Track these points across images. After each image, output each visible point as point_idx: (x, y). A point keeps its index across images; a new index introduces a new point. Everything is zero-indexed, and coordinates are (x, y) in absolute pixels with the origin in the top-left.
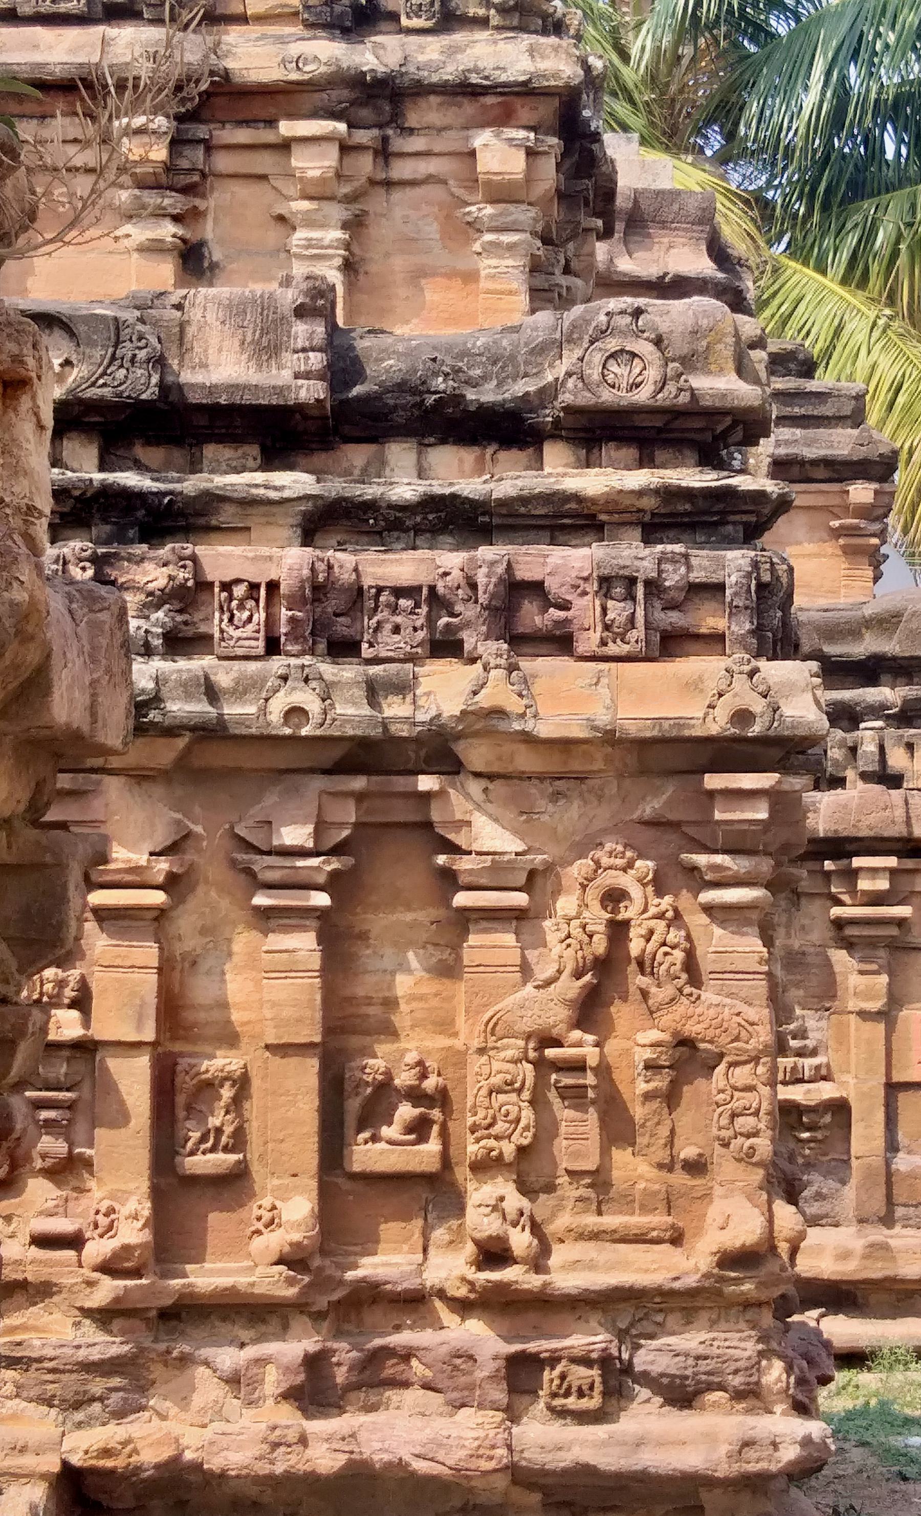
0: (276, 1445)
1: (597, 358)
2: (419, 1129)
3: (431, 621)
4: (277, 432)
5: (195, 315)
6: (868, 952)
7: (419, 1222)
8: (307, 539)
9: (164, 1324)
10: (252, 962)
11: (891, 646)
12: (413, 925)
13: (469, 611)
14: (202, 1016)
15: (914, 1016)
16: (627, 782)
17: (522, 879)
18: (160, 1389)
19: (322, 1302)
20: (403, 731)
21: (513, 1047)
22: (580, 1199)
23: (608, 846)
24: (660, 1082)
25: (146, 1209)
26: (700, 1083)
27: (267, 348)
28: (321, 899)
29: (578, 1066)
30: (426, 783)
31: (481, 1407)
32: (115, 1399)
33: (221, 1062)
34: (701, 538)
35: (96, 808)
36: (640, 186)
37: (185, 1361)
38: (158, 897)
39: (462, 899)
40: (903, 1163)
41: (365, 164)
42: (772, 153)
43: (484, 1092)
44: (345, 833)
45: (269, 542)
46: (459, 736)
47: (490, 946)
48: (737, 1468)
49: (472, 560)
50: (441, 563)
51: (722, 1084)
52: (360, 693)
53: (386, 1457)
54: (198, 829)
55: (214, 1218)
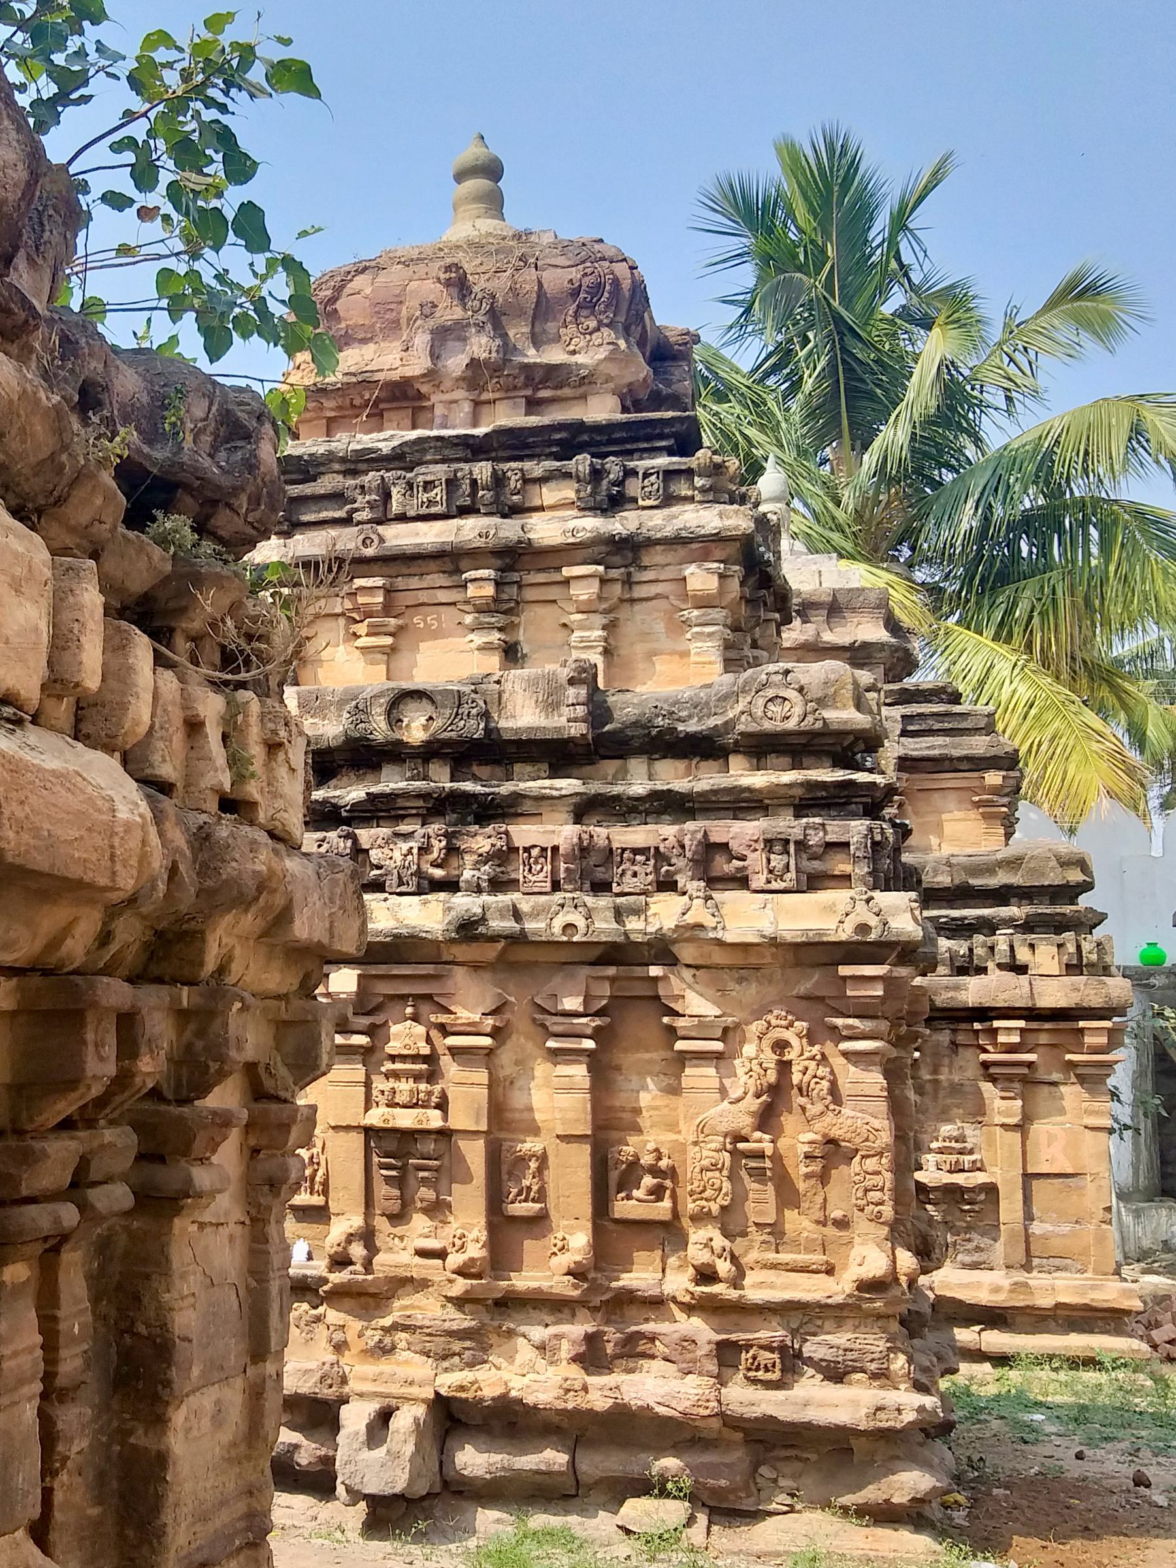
0: (568, 1391)
1: (761, 702)
2: (657, 1193)
3: (657, 869)
4: (557, 755)
5: (507, 686)
6: (1007, 1084)
7: (660, 1252)
8: (578, 820)
9: (496, 1309)
10: (547, 1083)
11: (1016, 879)
12: (649, 1062)
13: (680, 863)
14: (517, 1116)
15: (1039, 1129)
16: (789, 971)
17: (719, 1034)
18: (495, 1350)
19: (596, 1301)
20: (639, 938)
21: (716, 1142)
22: (763, 1242)
23: (776, 1012)
24: (816, 1167)
25: (484, 1236)
26: (843, 1167)
27: (551, 705)
28: (589, 1044)
29: (760, 1155)
30: (655, 971)
31: (700, 1374)
32: (467, 1355)
33: (531, 1145)
34: (833, 813)
35: (449, 986)
36: (837, 587)
37: (511, 1333)
38: (486, 1041)
39: (680, 1045)
40: (1036, 1228)
41: (617, 590)
42: (943, 556)
43: (697, 1170)
44: (604, 1002)
46: (675, 941)
47: (699, 1076)
48: (872, 1425)
49: (682, 830)
50: (664, 832)
51: (857, 1170)
52: (610, 914)
53: (640, 1403)
54: (512, 999)
55: (527, 1243)
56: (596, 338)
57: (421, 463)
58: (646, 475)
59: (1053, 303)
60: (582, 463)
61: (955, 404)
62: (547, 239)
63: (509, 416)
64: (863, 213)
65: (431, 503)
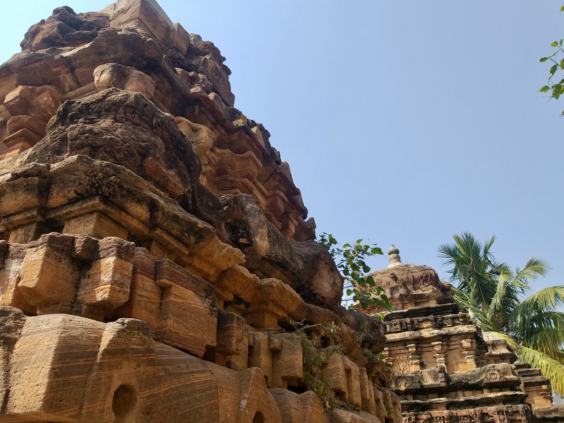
1: (489, 375)
5: (424, 374)
13: (476, 419)
27: (436, 378)
41: (446, 347)
42: (515, 329)
45: (442, 410)
56: (429, 287)
57: (393, 319)
58: (447, 319)
59: (527, 267)
60: (431, 317)
61: (509, 292)
62: (413, 266)
63: (410, 307)
64: (477, 250)
65: (397, 329)
